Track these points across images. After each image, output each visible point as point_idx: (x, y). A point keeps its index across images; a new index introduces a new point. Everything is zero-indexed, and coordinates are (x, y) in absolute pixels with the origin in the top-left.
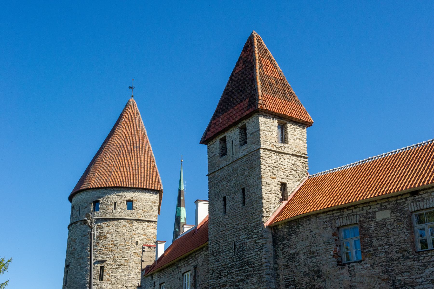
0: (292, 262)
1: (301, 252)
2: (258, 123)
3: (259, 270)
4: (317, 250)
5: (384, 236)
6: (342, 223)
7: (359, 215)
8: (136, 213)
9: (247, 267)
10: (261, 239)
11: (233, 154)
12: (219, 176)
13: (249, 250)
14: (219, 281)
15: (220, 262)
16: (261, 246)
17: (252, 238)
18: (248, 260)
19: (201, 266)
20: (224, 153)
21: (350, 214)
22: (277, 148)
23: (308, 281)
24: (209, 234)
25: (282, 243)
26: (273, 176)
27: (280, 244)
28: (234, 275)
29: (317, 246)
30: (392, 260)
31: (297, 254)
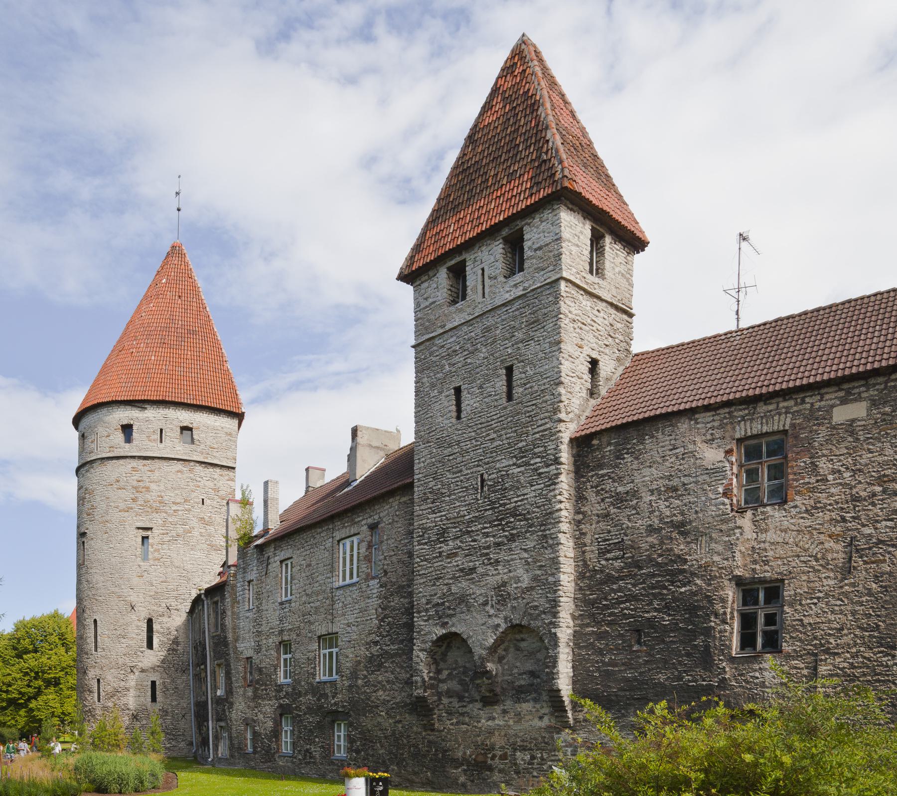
0: (619, 508)
2: (557, 224)
3: (541, 526)
5: (848, 453)
6: (749, 431)
7: (793, 414)
9: (512, 520)
10: (552, 464)
11: (484, 297)
12: (443, 346)
18: (515, 507)
21: (771, 411)
22: (587, 283)
25: (596, 474)
27: (592, 476)
30: (856, 499)
31: (635, 494)
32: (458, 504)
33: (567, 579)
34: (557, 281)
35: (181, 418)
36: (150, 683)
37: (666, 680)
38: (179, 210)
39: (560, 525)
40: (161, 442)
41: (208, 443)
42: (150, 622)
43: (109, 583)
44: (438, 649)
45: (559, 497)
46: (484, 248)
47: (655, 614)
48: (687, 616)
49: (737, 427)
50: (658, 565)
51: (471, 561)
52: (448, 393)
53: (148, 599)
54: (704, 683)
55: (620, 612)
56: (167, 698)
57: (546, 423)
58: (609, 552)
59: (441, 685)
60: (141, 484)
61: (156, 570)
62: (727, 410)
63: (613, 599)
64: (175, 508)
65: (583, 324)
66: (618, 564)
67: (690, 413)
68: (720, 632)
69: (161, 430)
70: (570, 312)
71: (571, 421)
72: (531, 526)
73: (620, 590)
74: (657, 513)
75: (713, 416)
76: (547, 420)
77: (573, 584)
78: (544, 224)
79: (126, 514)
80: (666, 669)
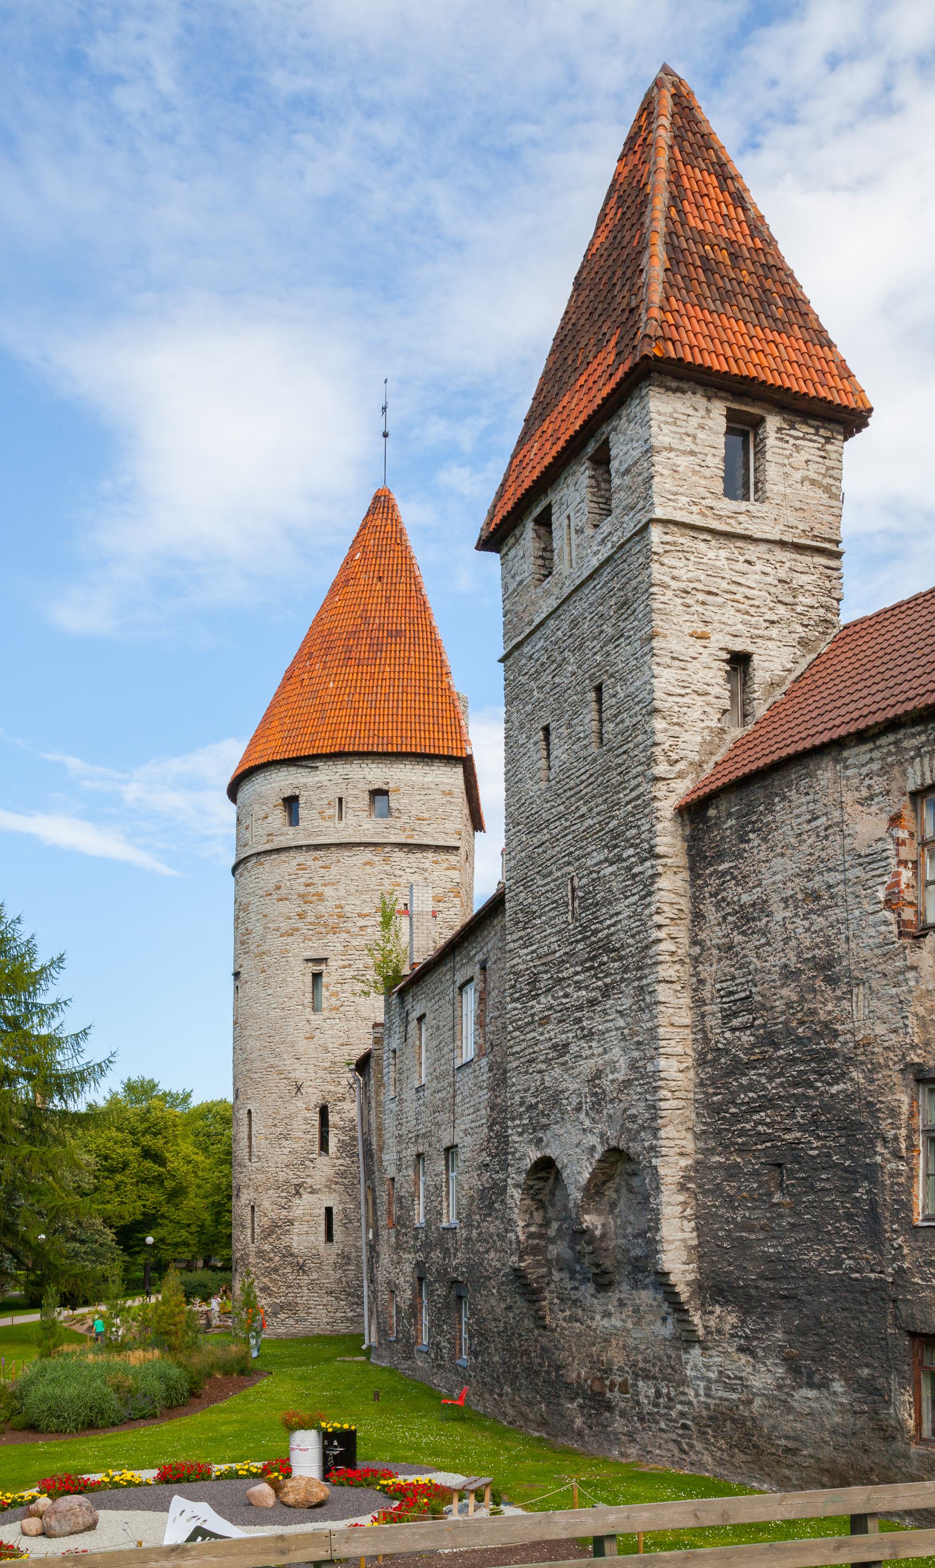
0: (744, 933)
1: (775, 897)
3: (640, 968)
6: (928, 774)
8: (398, 825)
9: (605, 959)
10: (646, 859)
12: (531, 658)
13: (610, 903)
14: (532, 1007)
15: (534, 947)
16: (645, 886)
17: (620, 859)
18: (607, 936)
19: (495, 963)
20: (546, 567)
22: (720, 517)
23: (794, 997)
25: (716, 871)
26: (700, 628)
27: (711, 875)
28: (569, 985)
29: (830, 870)
31: (762, 906)
32: (549, 931)
33: (676, 1067)
34: (645, 527)
35: (369, 777)
36: (323, 1211)
37: (820, 1263)
38: (385, 435)
39: (659, 968)
40: (341, 818)
41: (414, 813)
42: (324, 1112)
43: (266, 1052)
44: (541, 1184)
45: (657, 919)
47: (799, 1135)
48: (843, 1141)
49: (910, 770)
50: (799, 1041)
51: (564, 1032)
53: (321, 1073)
54: (872, 1275)
55: (753, 1129)
56: (349, 1235)
57: (639, 785)
58: (735, 1014)
59: (551, 1247)
60: (311, 889)
61: (332, 1026)
62: (891, 738)
63: (743, 1103)
64: (361, 922)
65: (709, 593)
66: (746, 1038)
67: (836, 746)
68: (891, 1175)
69: (340, 800)
70: (673, 578)
71: (681, 775)
72: (626, 970)
73: (751, 1087)
74: (793, 943)
75: (871, 750)
76: (640, 779)
77: (691, 1074)
78: (632, 424)
79: (290, 939)
80: (820, 1242)
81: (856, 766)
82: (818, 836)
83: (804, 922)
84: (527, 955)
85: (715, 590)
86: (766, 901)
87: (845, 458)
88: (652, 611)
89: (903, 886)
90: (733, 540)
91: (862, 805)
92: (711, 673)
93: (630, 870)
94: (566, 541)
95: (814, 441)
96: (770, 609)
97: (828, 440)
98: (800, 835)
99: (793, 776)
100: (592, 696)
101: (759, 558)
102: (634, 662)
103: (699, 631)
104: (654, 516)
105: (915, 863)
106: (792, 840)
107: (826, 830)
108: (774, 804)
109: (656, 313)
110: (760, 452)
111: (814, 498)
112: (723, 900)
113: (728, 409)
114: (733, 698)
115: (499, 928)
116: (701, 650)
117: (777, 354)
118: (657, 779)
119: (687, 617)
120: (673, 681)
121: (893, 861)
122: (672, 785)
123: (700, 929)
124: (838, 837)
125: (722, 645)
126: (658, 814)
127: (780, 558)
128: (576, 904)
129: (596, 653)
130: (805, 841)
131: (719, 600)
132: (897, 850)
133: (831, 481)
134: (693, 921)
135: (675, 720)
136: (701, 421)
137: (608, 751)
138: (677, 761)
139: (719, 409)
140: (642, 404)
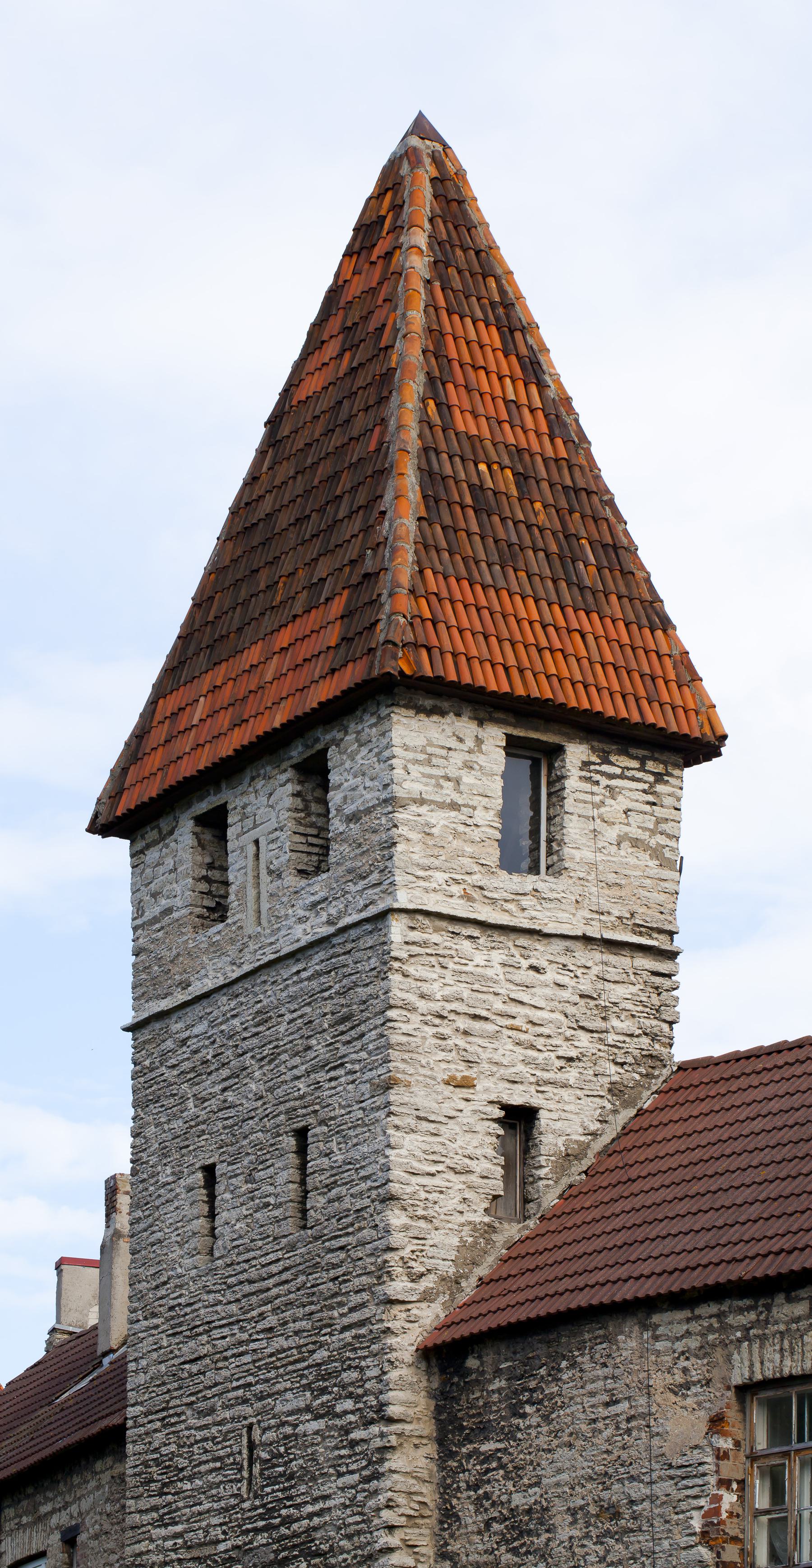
0: (515, 1551)
1: (559, 1506)
4: (632, 1502)
6: (757, 1366)
10: (372, 1422)
12: (184, 1042)
13: (314, 1479)
15: (179, 1528)
17: (329, 1412)
18: (308, 1530)
19: (96, 1537)
22: (493, 901)
24: (132, 1366)
25: (476, 1451)
26: (461, 1071)
27: (469, 1456)
29: (632, 1478)
31: (540, 1514)
32: (206, 1506)
34: (383, 915)
45: (387, 1515)
46: (260, 784)
49: (736, 1356)
52: (190, 1181)
57: (363, 1305)
62: (713, 1308)
65: (476, 1017)
70: (422, 996)
71: (427, 1297)
75: (688, 1320)
76: (365, 1296)
81: (668, 1339)
82: (618, 1428)
83: (598, 1548)
84: (165, 1539)
85: (484, 1013)
86: (547, 1509)
87: (683, 805)
88: (389, 1046)
89: (724, 1515)
90: (513, 936)
91: (676, 1394)
92: (475, 1140)
93: (347, 1432)
94: (250, 878)
95: (639, 780)
96: (567, 1039)
97: (659, 778)
98: (594, 1421)
99: (587, 1336)
100: (290, 1142)
101: (551, 962)
102: (360, 1114)
103: (459, 1075)
104: (396, 906)
105: (741, 1483)
106: (584, 1427)
107: (628, 1420)
108: (560, 1370)
109: (405, 603)
110: (557, 795)
111: (636, 867)
112: (487, 1496)
113: (509, 737)
114: (508, 1178)
115: (106, 1477)
116: (462, 1105)
117: (584, 653)
118: (392, 1302)
119: (442, 1055)
120: (418, 1153)
121: (713, 1480)
122: (414, 1311)
123: (452, 1536)
124: (643, 1435)
125: (493, 1097)
126: (392, 1356)
127: (583, 961)
128: (257, 1469)
129: (298, 1078)
130: (600, 1432)
131: (490, 1027)
132: (717, 1465)
133: (662, 840)
134: (441, 1522)
135: (420, 1212)
136: (467, 757)
137: (316, 1238)
138: (422, 1275)
139: (495, 737)
140: (382, 728)
